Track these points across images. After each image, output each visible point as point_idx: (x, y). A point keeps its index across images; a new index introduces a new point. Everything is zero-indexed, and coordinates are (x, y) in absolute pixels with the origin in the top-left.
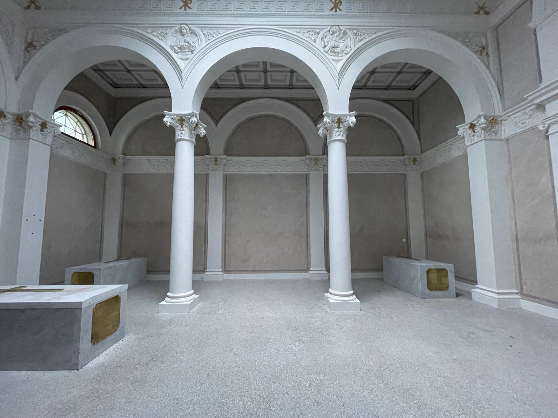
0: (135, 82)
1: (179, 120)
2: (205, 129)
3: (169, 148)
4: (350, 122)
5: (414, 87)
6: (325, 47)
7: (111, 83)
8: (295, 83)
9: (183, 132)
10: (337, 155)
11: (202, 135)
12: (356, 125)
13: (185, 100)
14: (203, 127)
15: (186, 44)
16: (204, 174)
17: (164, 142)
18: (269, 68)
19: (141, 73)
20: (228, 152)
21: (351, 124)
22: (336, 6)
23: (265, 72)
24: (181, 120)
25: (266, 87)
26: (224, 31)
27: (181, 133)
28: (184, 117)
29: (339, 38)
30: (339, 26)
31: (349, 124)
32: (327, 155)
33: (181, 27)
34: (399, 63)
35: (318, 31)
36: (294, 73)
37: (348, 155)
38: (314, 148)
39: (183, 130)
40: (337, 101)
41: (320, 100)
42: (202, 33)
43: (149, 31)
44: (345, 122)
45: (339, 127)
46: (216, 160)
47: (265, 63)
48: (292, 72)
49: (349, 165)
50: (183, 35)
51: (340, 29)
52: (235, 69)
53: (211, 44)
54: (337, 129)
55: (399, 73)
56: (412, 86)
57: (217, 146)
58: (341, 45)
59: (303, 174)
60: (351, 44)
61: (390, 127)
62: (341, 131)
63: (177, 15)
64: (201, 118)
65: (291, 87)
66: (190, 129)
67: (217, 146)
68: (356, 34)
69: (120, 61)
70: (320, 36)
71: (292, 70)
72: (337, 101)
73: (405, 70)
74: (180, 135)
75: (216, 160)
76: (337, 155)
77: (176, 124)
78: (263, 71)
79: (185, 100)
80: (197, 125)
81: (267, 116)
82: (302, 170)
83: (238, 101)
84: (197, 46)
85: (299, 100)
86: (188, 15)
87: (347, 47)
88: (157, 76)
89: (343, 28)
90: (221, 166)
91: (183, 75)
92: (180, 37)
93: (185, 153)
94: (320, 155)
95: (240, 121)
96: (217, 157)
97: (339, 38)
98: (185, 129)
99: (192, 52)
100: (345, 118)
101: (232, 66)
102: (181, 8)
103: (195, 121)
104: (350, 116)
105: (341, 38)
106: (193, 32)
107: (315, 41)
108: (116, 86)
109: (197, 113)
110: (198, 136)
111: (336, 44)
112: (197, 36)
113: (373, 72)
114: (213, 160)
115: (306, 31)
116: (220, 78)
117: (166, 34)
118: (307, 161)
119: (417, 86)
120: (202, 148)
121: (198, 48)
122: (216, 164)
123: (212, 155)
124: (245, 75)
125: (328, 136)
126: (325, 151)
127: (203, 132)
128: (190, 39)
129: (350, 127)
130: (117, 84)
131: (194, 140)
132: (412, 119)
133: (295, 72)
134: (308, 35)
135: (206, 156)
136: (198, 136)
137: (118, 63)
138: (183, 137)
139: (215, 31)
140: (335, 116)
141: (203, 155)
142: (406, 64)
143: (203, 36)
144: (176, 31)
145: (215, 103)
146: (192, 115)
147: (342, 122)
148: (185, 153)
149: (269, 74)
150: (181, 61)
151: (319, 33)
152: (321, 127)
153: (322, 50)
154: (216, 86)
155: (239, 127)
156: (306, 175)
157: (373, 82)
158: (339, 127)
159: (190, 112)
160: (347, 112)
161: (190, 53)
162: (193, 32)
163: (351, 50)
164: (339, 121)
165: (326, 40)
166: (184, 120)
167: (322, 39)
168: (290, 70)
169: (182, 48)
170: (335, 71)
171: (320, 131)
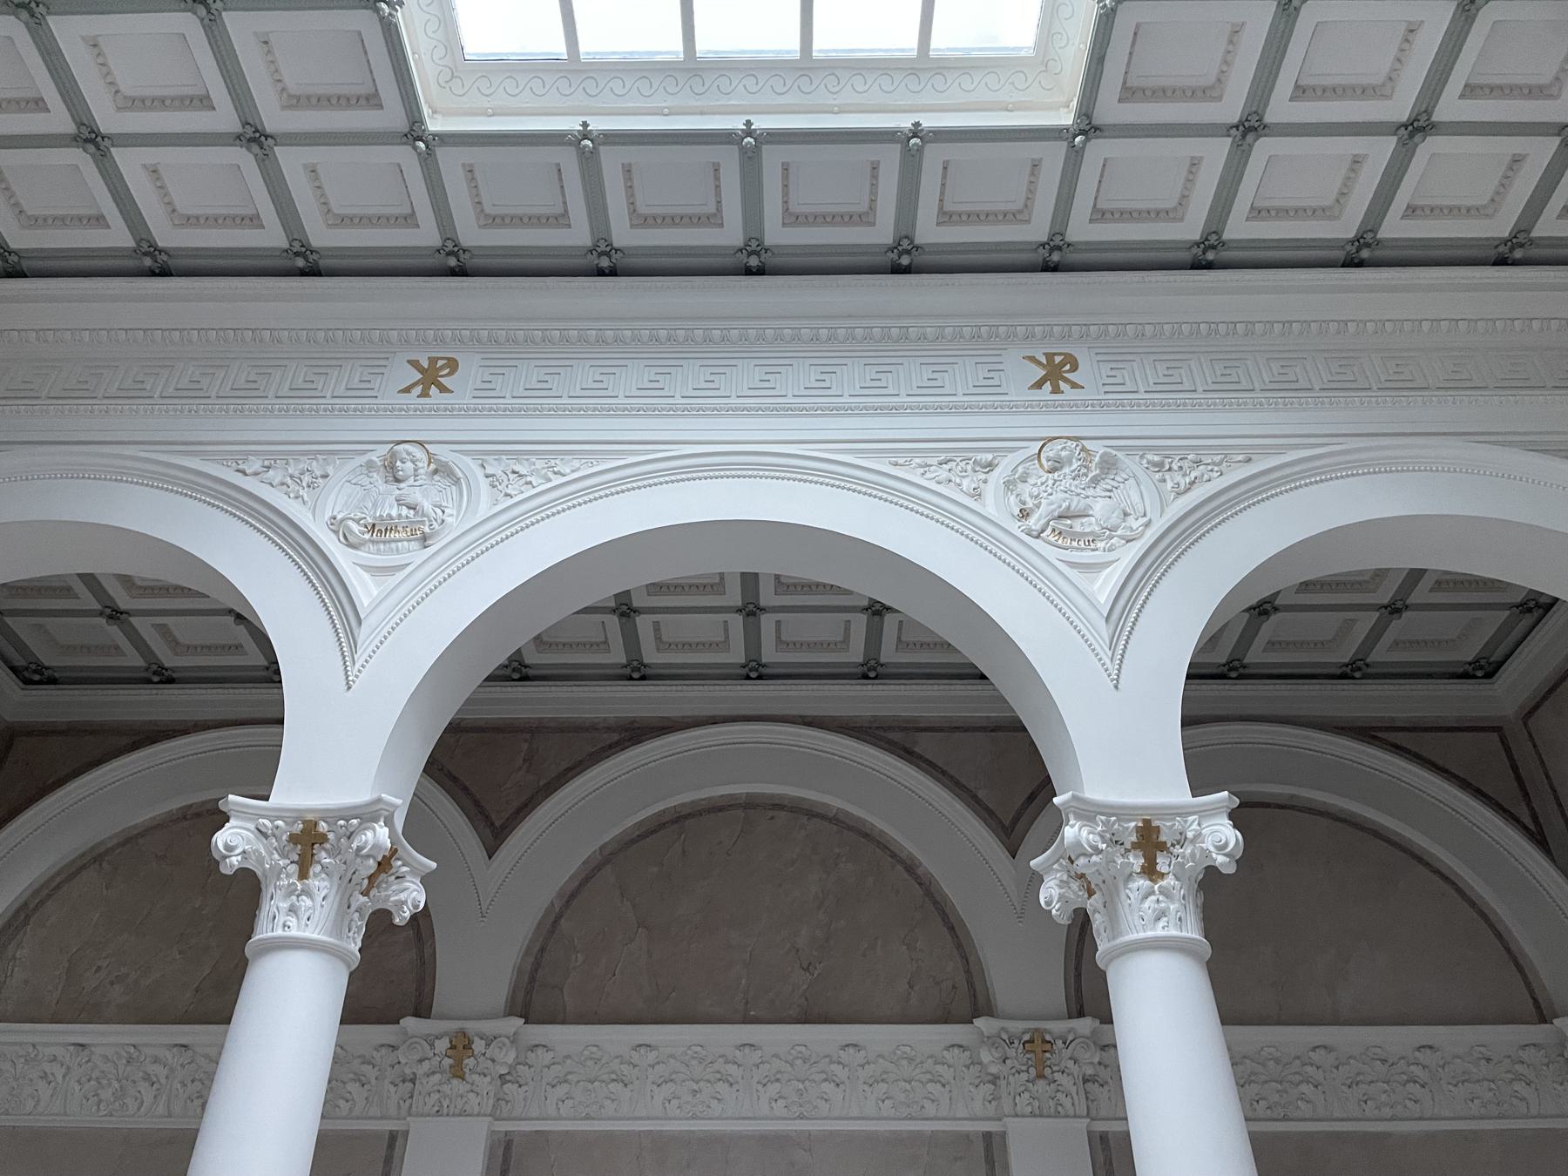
0: (133, 660)
1: (294, 839)
2: (427, 881)
3: (209, 989)
4: (1208, 845)
5: (1486, 669)
6: (1024, 514)
7: (19, 662)
8: (889, 654)
9: (306, 902)
10: (1163, 1016)
11: (402, 917)
12: (1245, 861)
13: (350, 735)
14: (413, 872)
15: (405, 511)
16: (375, 1135)
17: (195, 952)
18: (767, 597)
19: (168, 620)
20: (533, 1001)
21: (1220, 859)
22: (1055, 373)
23: (751, 611)
24: (307, 840)
25: (754, 671)
26: (576, 464)
27: (293, 910)
28: (323, 827)
29: (1085, 480)
30: (1077, 439)
31: (1206, 854)
32: (1108, 1019)
33: (393, 456)
34: (1380, 574)
35: (990, 457)
36: (888, 617)
37: (1228, 1017)
38: (1022, 979)
39: (306, 892)
40: (1120, 741)
41: (1025, 729)
42: (479, 473)
43: (255, 465)
44: (1182, 841)
45: (1150, 871)
46: (461, 1045)
47: (750, 581)
48: (877, 610)
49: (1248, 1075)
50: (397, 481)
51: (1083, 449)
52: (613, 604)
53: (515, 512)
54: (1143, 883)
55: (1394, 609)
56: (1475, 663)
57: (475, 972)
58: (1099, 507)
59: (967, 1137)
60: (1143, 504)
61: (1419, 858)
62: (1164, 892)
63: (392, 411)
64: (418, 828)
65: (871, 671)
66: (347, 882)
67: (475, 972)
68: (1160, 465)
69: (89, 580)
70: (998, 476)
71: (874, 602)
72: (1120, 741)
73: (1418, 596)
74: (280, 920)
75: (461, 1045)
76: (1163, 1016)
77: (273, 861)
78: (739, 610)
79: (350, 735)
80: (384, 865)
81: (751, 804)
82: (959, 1110)
83: (615, 737)
84: (449, 520)
85: (915, 727)
86: (435, 412)
87: (1126, 514)
88: (241, 632)
89: (1098, 448)
90: (483, 1083)
91: (362, 634)
92: (382, 487)
93: (291, 1010)
94: (1058, 1018)
95: (616, 831)
96: (471, 1026)
97: (1085, 480)
98: (320, 884)
99: (424, 540)
100: (1178, 823)
101: (604, 592)
102: (407, 390)
103: (376, 846)
104: (1205, 813)
105: (1095, 481)
106: (442, 470)
107: (977, 494)
108: (33, 675)
109: (400, 803)
110: (379, 923)
111: (1076, 504)
112: (457, 482)
113: (1263, 609)
114: (442, 1045)
115: (934, 461)
116: (538, 639)
117: (325, 476)
118: (985, 1056)
119: (1500, 664)
120: (391, 980)
121: (455, 522)
122: (458, 1072)
123: (442, 1017)
124: (657, 626)
125: (1098, 921)
126: (1088, 995)
127: (409, 896)
128: (425, 493)
129: (1211, 871)
130: (40, 668)
131: (354, 946)
132: (1527, 821)
133: (888, 609)
134: (944, 475)
135: (410, 1023)
136: (379, 923)
137: (80, 588)
138: (294, 932)
139: (539, 464)
140: (1120, 812)
141: (389, 1017)
142: (1416, 575)
143: (484, 484)
144: (370, 465)
145: (495, 750)
146: (368, 814)
147: (1162, 847)
148: (291, 1010)
149: (767, 622)
150: (366, 576)
151: (990, 466)
152: (1049, 869)
153: (1015, 527)
154: (516, 671)
155: (608, 857)
156: (987, 1137)
157: (1271, 645)
158: (1150, 871)
159: (361, 796)
160: (1180, 793)
161: (414, 545)
162: (442, 470)
163: (1147, 525)
164: (1150, 840)
165: (1026, 490)
166: (323, 839)
167: (1009, 485)
168: (865, 603)
169: (379, 529)
170: (1093, 614)
171: (1051, 892)
